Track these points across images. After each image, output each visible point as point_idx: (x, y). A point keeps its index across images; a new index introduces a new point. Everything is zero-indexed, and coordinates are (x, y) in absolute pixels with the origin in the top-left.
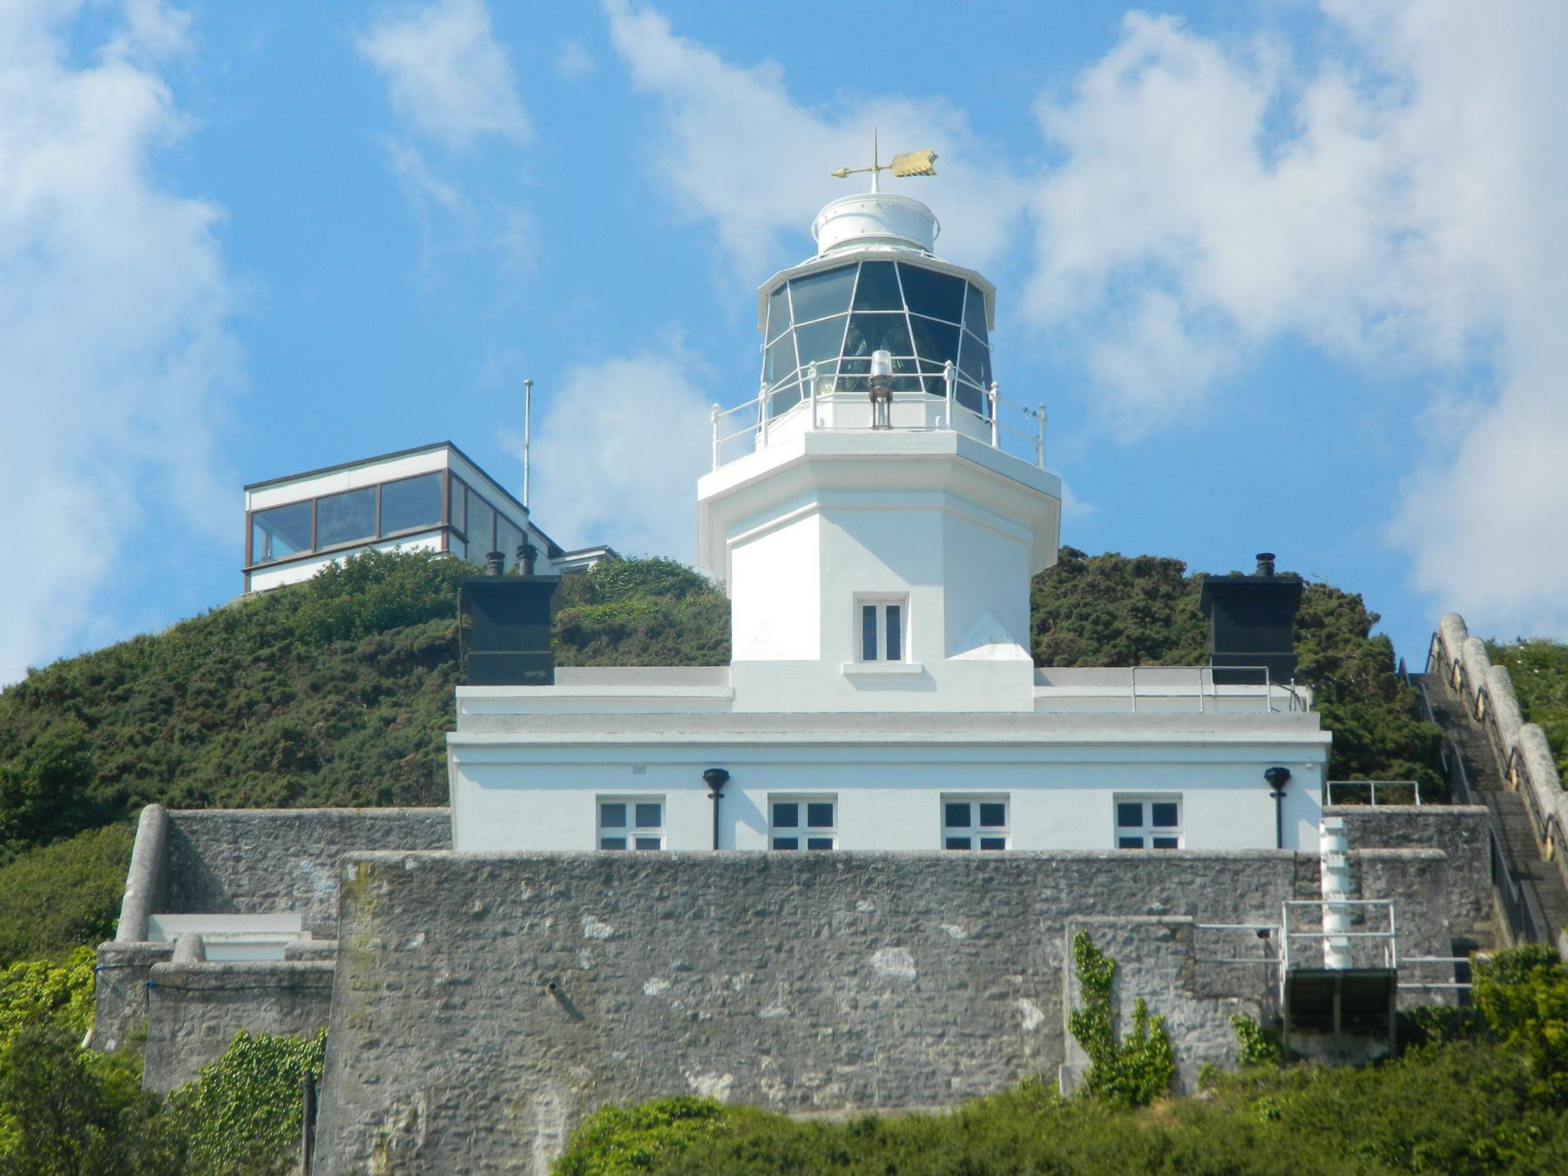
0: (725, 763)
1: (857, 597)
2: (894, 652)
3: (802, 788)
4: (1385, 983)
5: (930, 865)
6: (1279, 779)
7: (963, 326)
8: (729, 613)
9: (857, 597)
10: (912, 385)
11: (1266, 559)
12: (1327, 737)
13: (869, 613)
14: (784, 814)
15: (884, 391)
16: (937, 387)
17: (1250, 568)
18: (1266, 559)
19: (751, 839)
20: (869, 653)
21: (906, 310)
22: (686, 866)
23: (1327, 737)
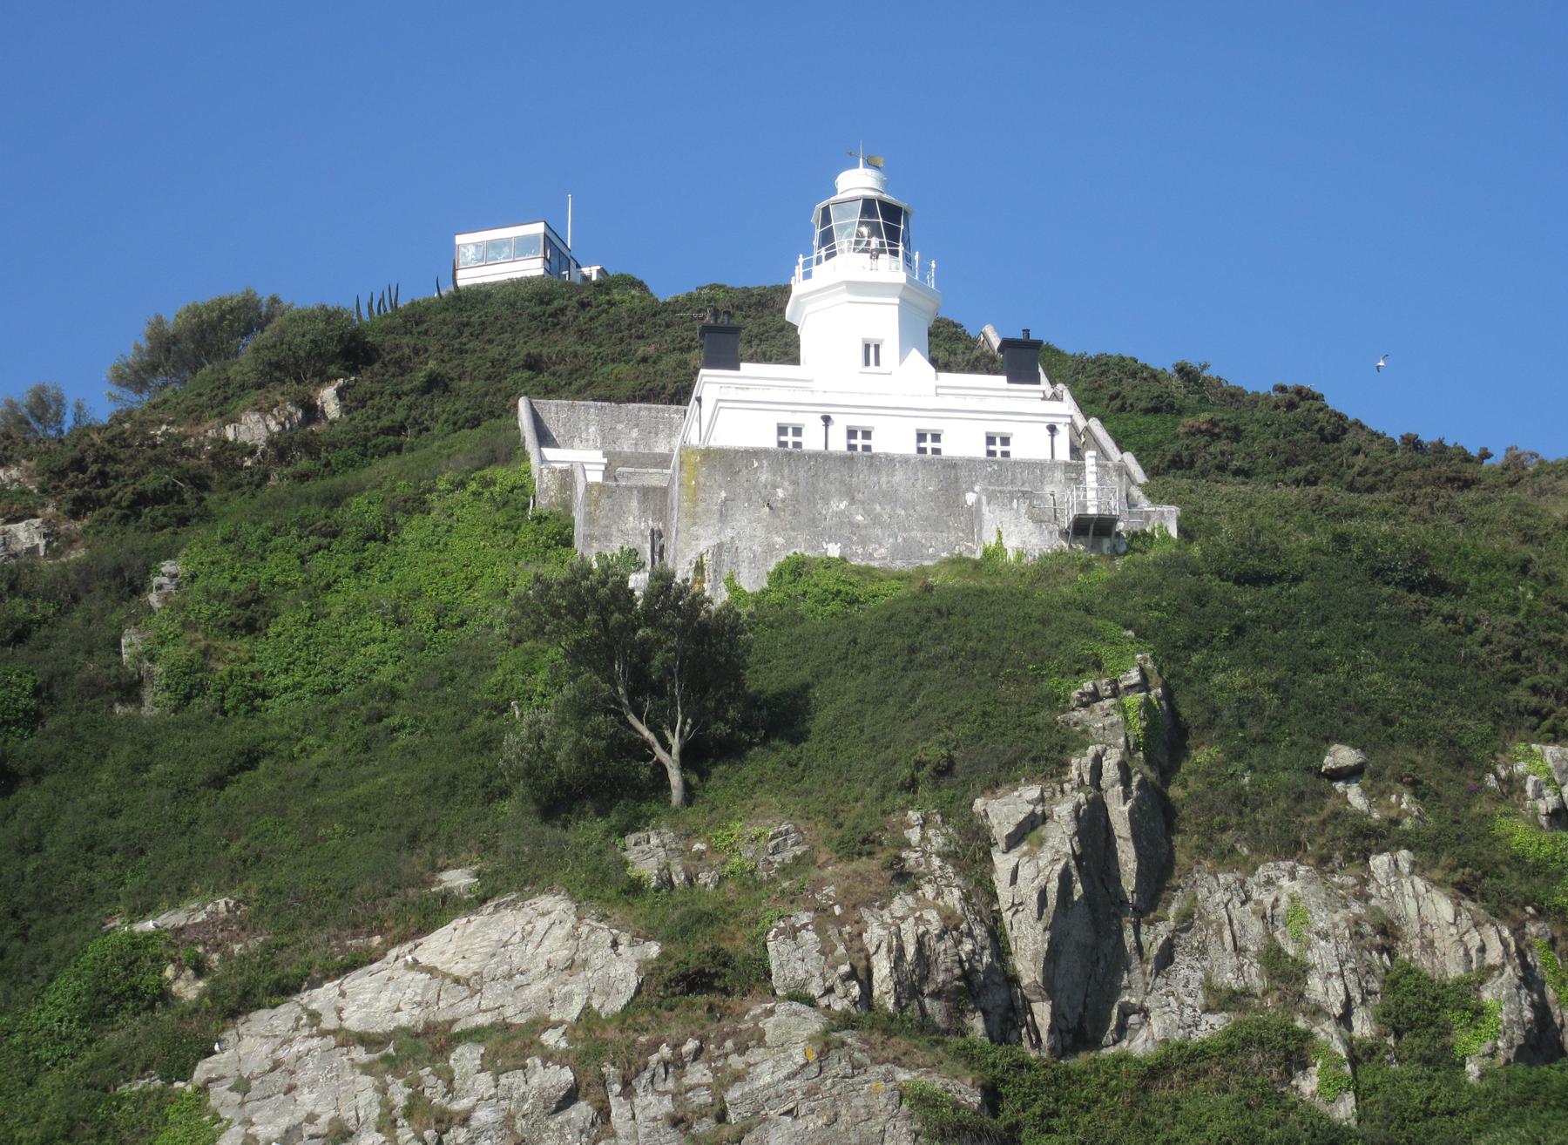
0: (1008, 390)
1: (864, 340)
2: (877, 363)
3: (859, 422)
4: (1113, 521)
5: (905, 460)
6: (1052, 429)
7: (902, 227)
8: (798, 347)
9: (864, 340)
10: (884, 252)
11: (1026, 331)
12: (605, 460)
13: (867, 347)
14: (852, 433)
15: (875, 254)
16: (895, 253)
17: (1020, 336)
18: (1026, 331)
19: (839, 444)
20: (867, 363)
21: (881, 220)
22: (815, 456)
23: (605, 460)
